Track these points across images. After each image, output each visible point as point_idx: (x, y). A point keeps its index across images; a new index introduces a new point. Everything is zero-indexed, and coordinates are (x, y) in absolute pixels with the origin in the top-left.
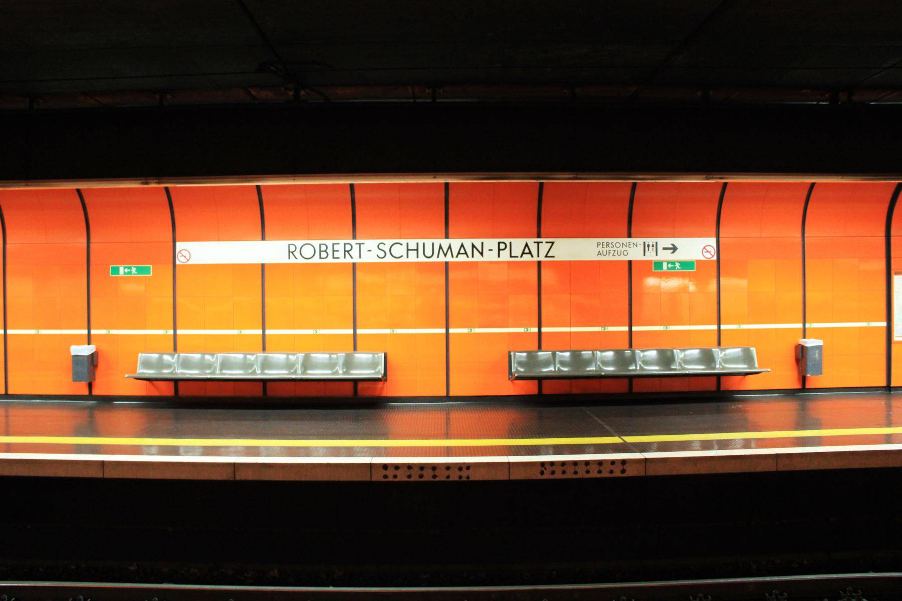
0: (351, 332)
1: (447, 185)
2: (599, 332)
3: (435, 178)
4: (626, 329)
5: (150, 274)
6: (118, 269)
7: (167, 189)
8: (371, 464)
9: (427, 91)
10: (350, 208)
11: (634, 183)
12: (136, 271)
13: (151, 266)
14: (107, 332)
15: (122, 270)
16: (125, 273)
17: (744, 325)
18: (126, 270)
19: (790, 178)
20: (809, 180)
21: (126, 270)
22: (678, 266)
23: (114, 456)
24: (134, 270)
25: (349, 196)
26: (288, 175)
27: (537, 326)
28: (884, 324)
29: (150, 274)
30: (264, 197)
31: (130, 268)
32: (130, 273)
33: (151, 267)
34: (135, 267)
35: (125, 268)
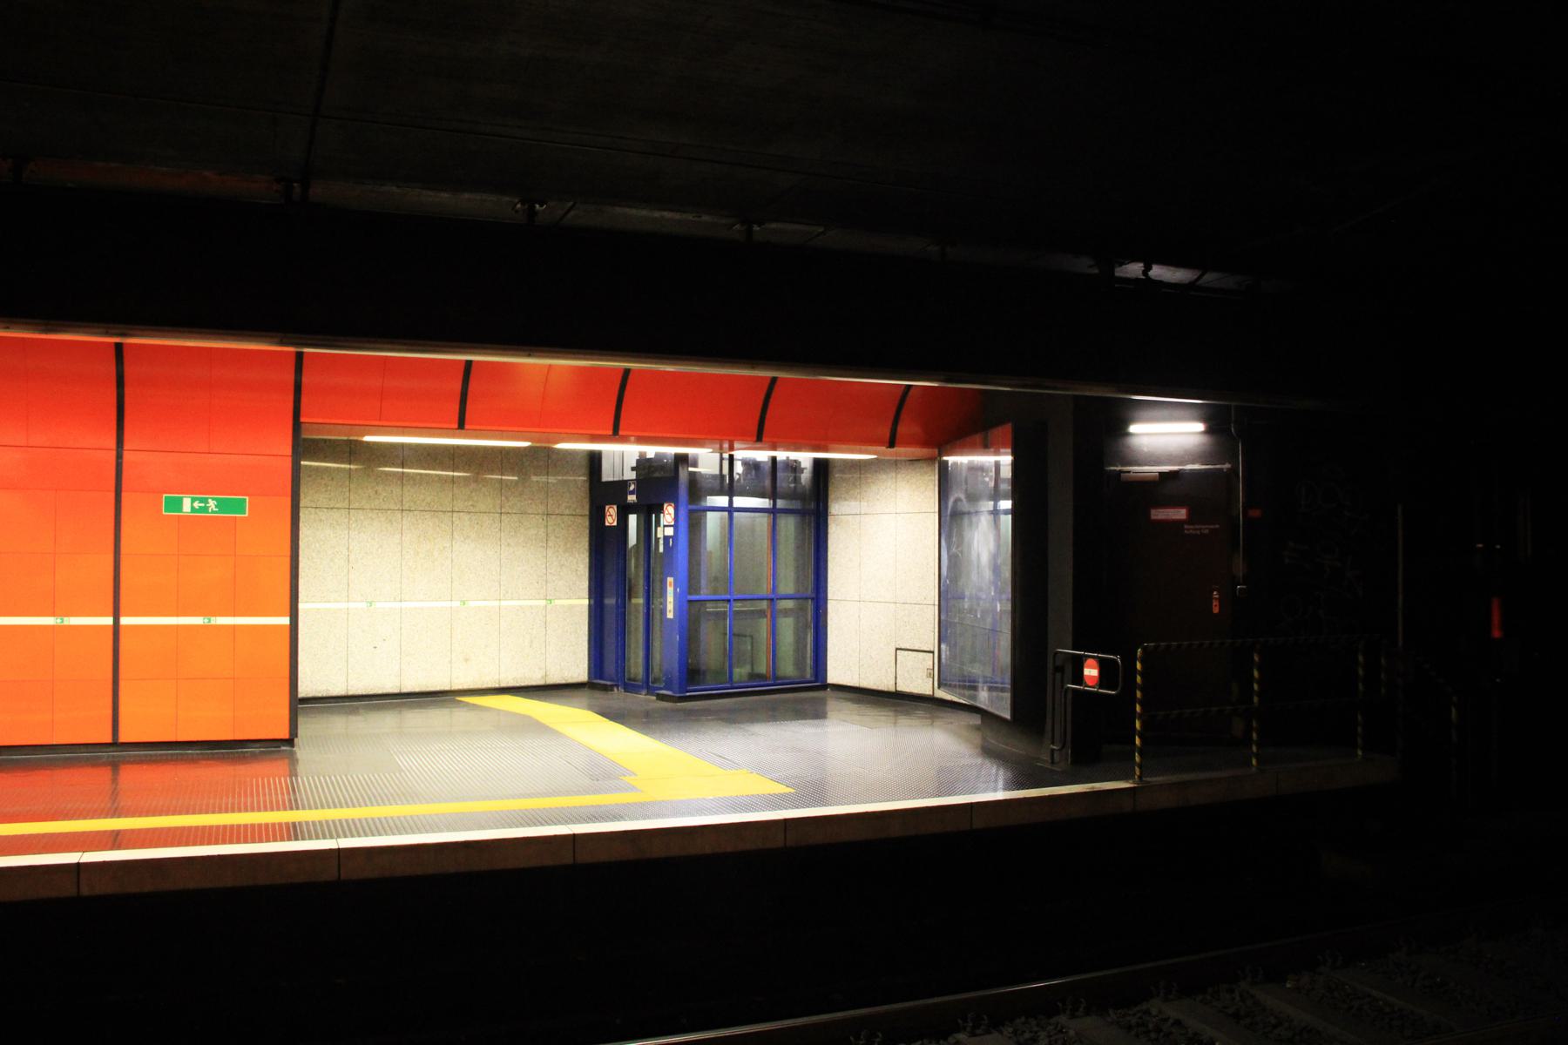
0: (109, 621)
1: (469, 363)
2: (53, 627)
3: (8, 328)
4: (108, 621)
5: (245, 513)
6: (180, 503)
7: (119, 348)
8: (78, 864)
9: (737, 227)
10: (291, 398)
11: (467, 361)
12: (216, 507)
13: (247, 498)
14: (206, 621)
15: (187, 504)
16: (193, 509)
17: (218, 618)
18: (196, 505)
19: (697, 365)
20: (767, 374)
21: (196, 505)
22: (213, 507)
23: (1021, 796)
24: (212, 504)
25: (290, 377)
26: (489, 351)
27: (111, 614)
28: (286, 621)
29: (245, 513)
30: (129, 371)
31: (206, 501)
32: (206, 509)
33: (247, 501)
34: (213, 499)
35: (193, 500)
